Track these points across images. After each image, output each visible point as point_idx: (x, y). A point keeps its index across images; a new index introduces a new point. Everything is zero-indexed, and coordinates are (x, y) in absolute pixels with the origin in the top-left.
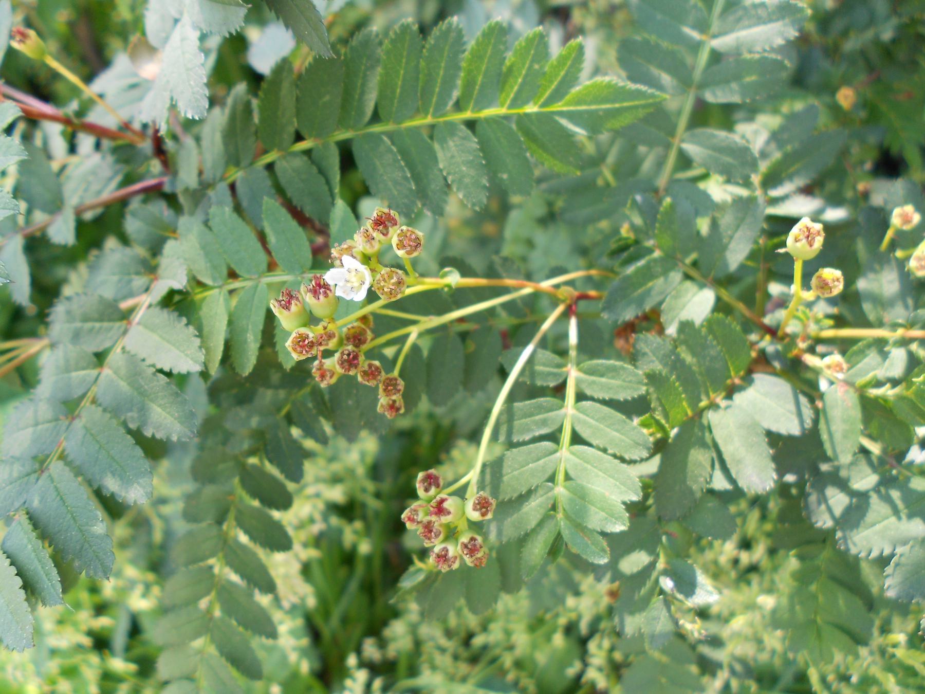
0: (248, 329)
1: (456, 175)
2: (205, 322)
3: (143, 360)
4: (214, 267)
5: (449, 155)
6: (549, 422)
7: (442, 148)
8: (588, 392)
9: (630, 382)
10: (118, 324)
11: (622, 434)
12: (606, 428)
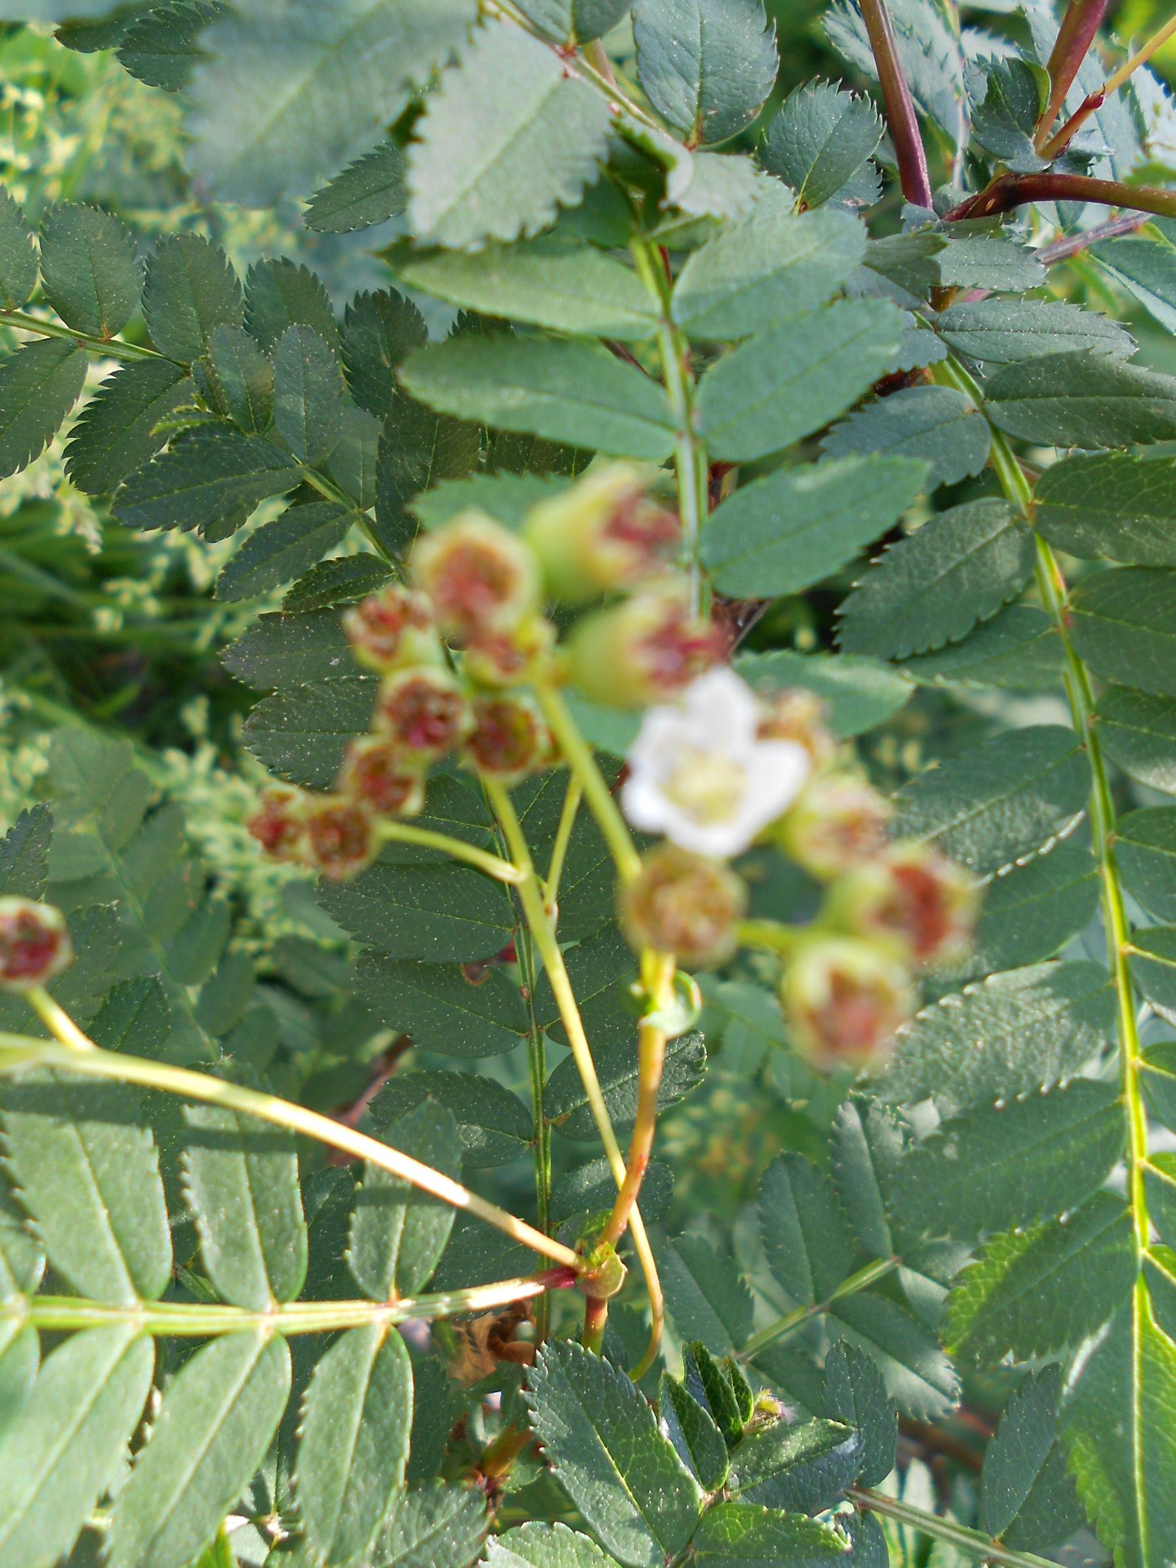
0: (539, 391)
1: (962, 1020)
2: (565, 264)
3: (454, 62)
4: (725, 304)
5: (1021, 1000)
6: (235, 1262)
7: (1042, 984)
8: (322, 1369)
9: (345, 1507)
10: (567, 18)
11: (186, 1493)
12: (207, 1440)
